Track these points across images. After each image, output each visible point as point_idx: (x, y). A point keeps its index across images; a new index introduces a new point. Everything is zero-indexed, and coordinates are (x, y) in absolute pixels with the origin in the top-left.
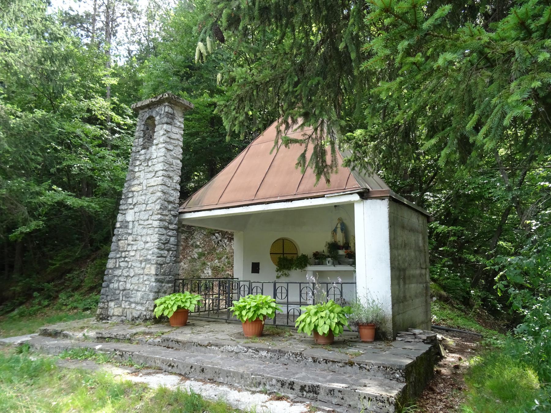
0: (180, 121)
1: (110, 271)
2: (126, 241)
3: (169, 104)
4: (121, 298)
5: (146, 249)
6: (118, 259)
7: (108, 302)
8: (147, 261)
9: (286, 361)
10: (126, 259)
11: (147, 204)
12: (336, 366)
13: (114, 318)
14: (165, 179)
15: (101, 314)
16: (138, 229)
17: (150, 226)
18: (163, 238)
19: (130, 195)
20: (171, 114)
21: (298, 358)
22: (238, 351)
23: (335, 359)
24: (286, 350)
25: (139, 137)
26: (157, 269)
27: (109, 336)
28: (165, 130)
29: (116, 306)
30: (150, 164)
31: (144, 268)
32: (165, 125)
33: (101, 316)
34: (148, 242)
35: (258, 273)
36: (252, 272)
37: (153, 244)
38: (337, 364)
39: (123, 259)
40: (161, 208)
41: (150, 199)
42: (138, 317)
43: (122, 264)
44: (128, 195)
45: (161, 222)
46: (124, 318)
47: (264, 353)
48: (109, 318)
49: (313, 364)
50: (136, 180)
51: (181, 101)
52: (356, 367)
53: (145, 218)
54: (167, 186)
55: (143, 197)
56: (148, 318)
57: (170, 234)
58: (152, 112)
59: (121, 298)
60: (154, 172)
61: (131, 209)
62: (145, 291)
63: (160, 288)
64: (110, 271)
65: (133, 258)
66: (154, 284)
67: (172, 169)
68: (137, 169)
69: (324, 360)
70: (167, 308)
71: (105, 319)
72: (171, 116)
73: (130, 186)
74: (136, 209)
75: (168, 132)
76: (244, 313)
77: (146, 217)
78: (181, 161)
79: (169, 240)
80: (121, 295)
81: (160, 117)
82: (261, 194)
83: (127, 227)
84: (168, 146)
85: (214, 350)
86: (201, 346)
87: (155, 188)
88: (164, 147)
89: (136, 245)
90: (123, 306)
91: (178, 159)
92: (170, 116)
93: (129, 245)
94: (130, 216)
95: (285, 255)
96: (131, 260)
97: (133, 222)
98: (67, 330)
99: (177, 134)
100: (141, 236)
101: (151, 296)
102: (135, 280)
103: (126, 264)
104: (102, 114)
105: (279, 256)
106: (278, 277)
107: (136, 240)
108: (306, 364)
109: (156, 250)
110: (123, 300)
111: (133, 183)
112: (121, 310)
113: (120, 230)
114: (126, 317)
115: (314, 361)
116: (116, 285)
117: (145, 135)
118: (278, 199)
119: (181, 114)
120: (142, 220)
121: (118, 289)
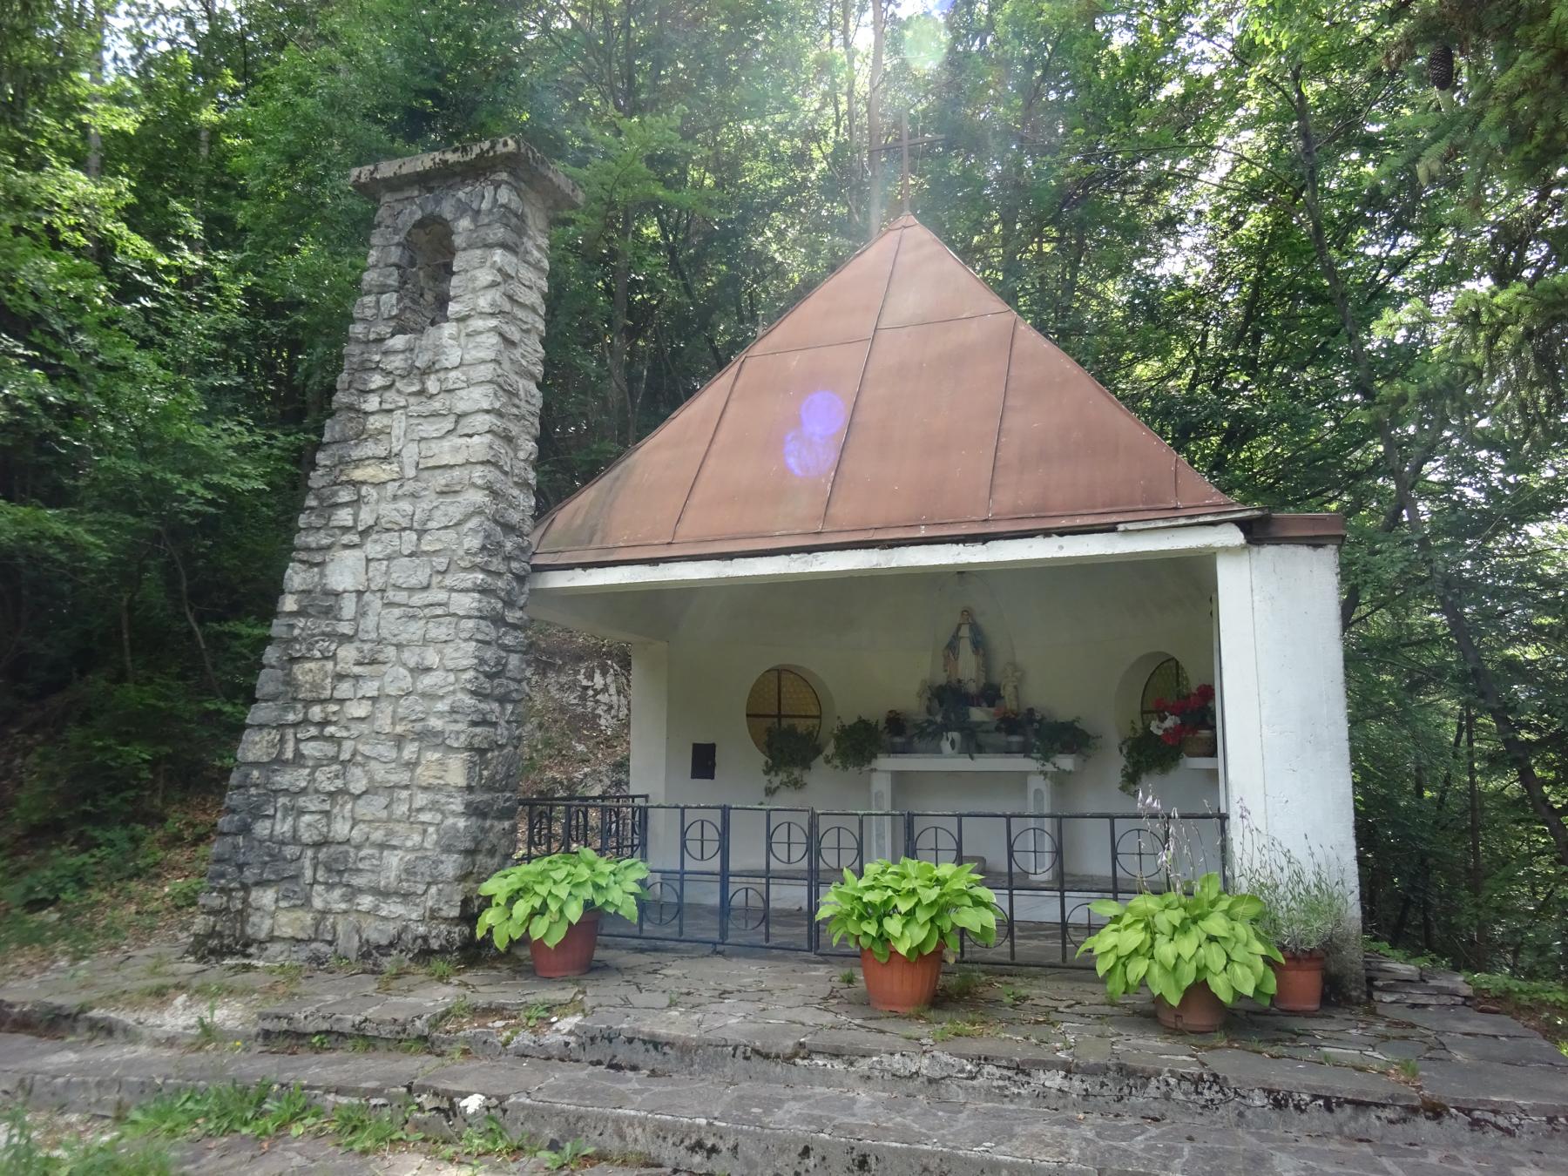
0: (537, 244)
1: (256, 773)
2: (330, 665)
3: (511, 180)
4: (308, 873)
5: (423, 695)
6: (290, 733)
7: (245, 888)
8: (426, 737)
9: (1155, 1105)
10: (330, 730)
11: (421, 533)
12: (1372, 1121)
13: (274, 948)
14: (497, 443)
15: (213, 933)
16: (382, 621)
17: (439, 611)
18: (490, 654)
19: (345, 496)
20: (516, 215)
21: (1208, 1094)
22: (937, 1074)
23: (1366, 1094)
24: (1150, 1067)
25: (383, 289)
26: (471, 767)
27: (325, 1026)
28: (500, 270)
29: (283, 904)
30: (432, 385)
31: (412, 765)
32: (499, 251)
33: (214, 943)
34: (428, 670)
35: (712, 777)
36: (693, 777)
37: (452, 678)
38: (1372, 1115)
39: (313, 731)
40: (483, 548)
41: (437, 513)
42: (391, 945)
43: (308, 749)
44: (334, 494)
45: (485, 599)
46: (324, 948)
47: (1055, 1080)
48: (252, 950)
49: (1274, 1116)
50: (370, 444)
51: (551, 175)
52: (1455, 1124)
53: (413, 582)
54: (500, 468)
55: (406, 506)
56: (435, 944)
57: (508, 640)
58: (438, 202)
59: (308, 873)
60: (452, 418)
61: (346, 547)
62: (421, 848)
63: (481, 836)
64: (256, 773)
65: (364, 727)
66: (462, 823)
67: (515, 411)
68: (372, 403)
69: (1315, 1097)
70: (542, 910)
71: (232, 953)
72: (516, 222)
73: (343, 462)
74: (373, 548)
75: (507, 277)
76: (893, 926)
77: (421, 577)
78: (539, 386)
79: (505, 665)
80: (307, 863)
81: (474, 220)
82: (684, 530)
83: (330, 612)
84: (505, 328)
85: (824, 1071)
86: (767, 1056)
87: (456, 473)
88: (495, 329)
89: (372, 678)
90: (318, 903)
91: (532, 376)
92: (514, 220)
93: (340, 677)
94: (344, 572)
95: (785, 723)
96: (355, 732)
97: (360, 593)
98: (101, 1002)
99: (530, 288)
100: (399, 646)
101: (450, 866)
102: (372, 808)
103: (330, 749)
104: (76, 227)
105: (769, 722)
106: (770, 792)
107: (373, 662)
108: (1241, 1115)
109: (469, 701)
110: (315, 881)
111: (356, 454)
112: (308, 919)
113: (301, 622)
114: (330, 943)
115: (1279, 1104)
116: (283, 827)
117: (403, 282)
118: (923, 532)
119: (542, 224)
120: (398, 588)
121: (295, 839)
